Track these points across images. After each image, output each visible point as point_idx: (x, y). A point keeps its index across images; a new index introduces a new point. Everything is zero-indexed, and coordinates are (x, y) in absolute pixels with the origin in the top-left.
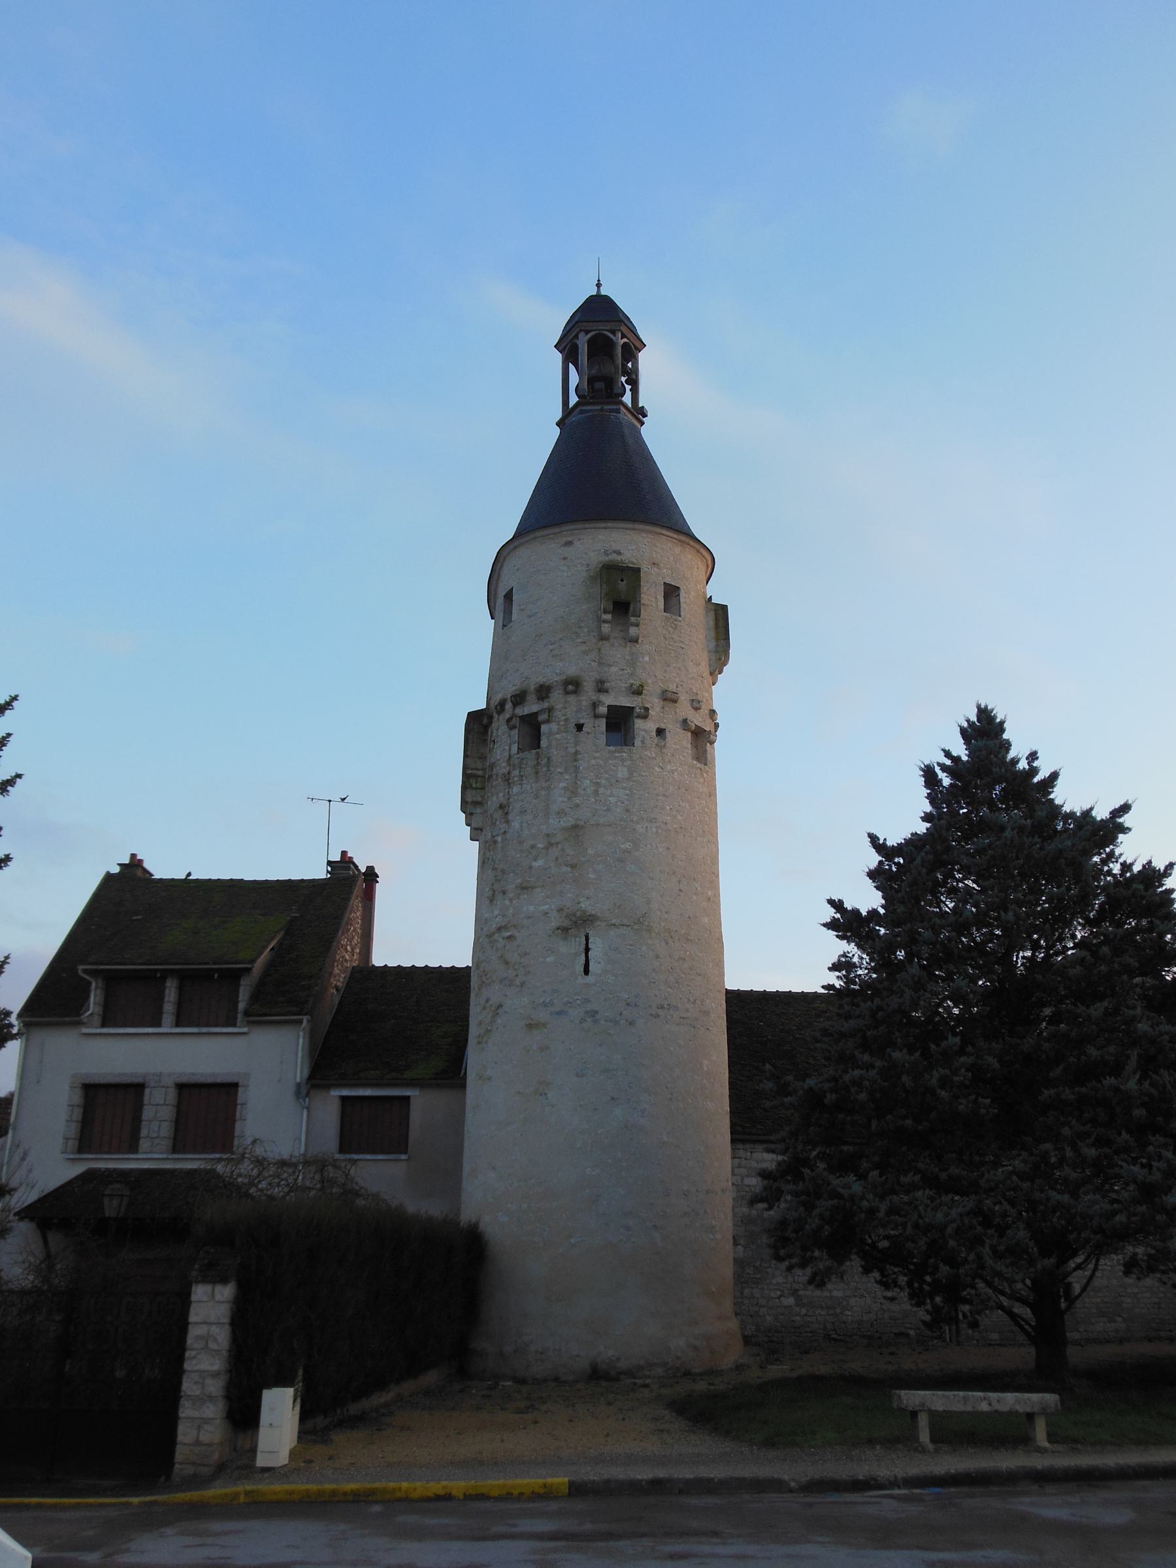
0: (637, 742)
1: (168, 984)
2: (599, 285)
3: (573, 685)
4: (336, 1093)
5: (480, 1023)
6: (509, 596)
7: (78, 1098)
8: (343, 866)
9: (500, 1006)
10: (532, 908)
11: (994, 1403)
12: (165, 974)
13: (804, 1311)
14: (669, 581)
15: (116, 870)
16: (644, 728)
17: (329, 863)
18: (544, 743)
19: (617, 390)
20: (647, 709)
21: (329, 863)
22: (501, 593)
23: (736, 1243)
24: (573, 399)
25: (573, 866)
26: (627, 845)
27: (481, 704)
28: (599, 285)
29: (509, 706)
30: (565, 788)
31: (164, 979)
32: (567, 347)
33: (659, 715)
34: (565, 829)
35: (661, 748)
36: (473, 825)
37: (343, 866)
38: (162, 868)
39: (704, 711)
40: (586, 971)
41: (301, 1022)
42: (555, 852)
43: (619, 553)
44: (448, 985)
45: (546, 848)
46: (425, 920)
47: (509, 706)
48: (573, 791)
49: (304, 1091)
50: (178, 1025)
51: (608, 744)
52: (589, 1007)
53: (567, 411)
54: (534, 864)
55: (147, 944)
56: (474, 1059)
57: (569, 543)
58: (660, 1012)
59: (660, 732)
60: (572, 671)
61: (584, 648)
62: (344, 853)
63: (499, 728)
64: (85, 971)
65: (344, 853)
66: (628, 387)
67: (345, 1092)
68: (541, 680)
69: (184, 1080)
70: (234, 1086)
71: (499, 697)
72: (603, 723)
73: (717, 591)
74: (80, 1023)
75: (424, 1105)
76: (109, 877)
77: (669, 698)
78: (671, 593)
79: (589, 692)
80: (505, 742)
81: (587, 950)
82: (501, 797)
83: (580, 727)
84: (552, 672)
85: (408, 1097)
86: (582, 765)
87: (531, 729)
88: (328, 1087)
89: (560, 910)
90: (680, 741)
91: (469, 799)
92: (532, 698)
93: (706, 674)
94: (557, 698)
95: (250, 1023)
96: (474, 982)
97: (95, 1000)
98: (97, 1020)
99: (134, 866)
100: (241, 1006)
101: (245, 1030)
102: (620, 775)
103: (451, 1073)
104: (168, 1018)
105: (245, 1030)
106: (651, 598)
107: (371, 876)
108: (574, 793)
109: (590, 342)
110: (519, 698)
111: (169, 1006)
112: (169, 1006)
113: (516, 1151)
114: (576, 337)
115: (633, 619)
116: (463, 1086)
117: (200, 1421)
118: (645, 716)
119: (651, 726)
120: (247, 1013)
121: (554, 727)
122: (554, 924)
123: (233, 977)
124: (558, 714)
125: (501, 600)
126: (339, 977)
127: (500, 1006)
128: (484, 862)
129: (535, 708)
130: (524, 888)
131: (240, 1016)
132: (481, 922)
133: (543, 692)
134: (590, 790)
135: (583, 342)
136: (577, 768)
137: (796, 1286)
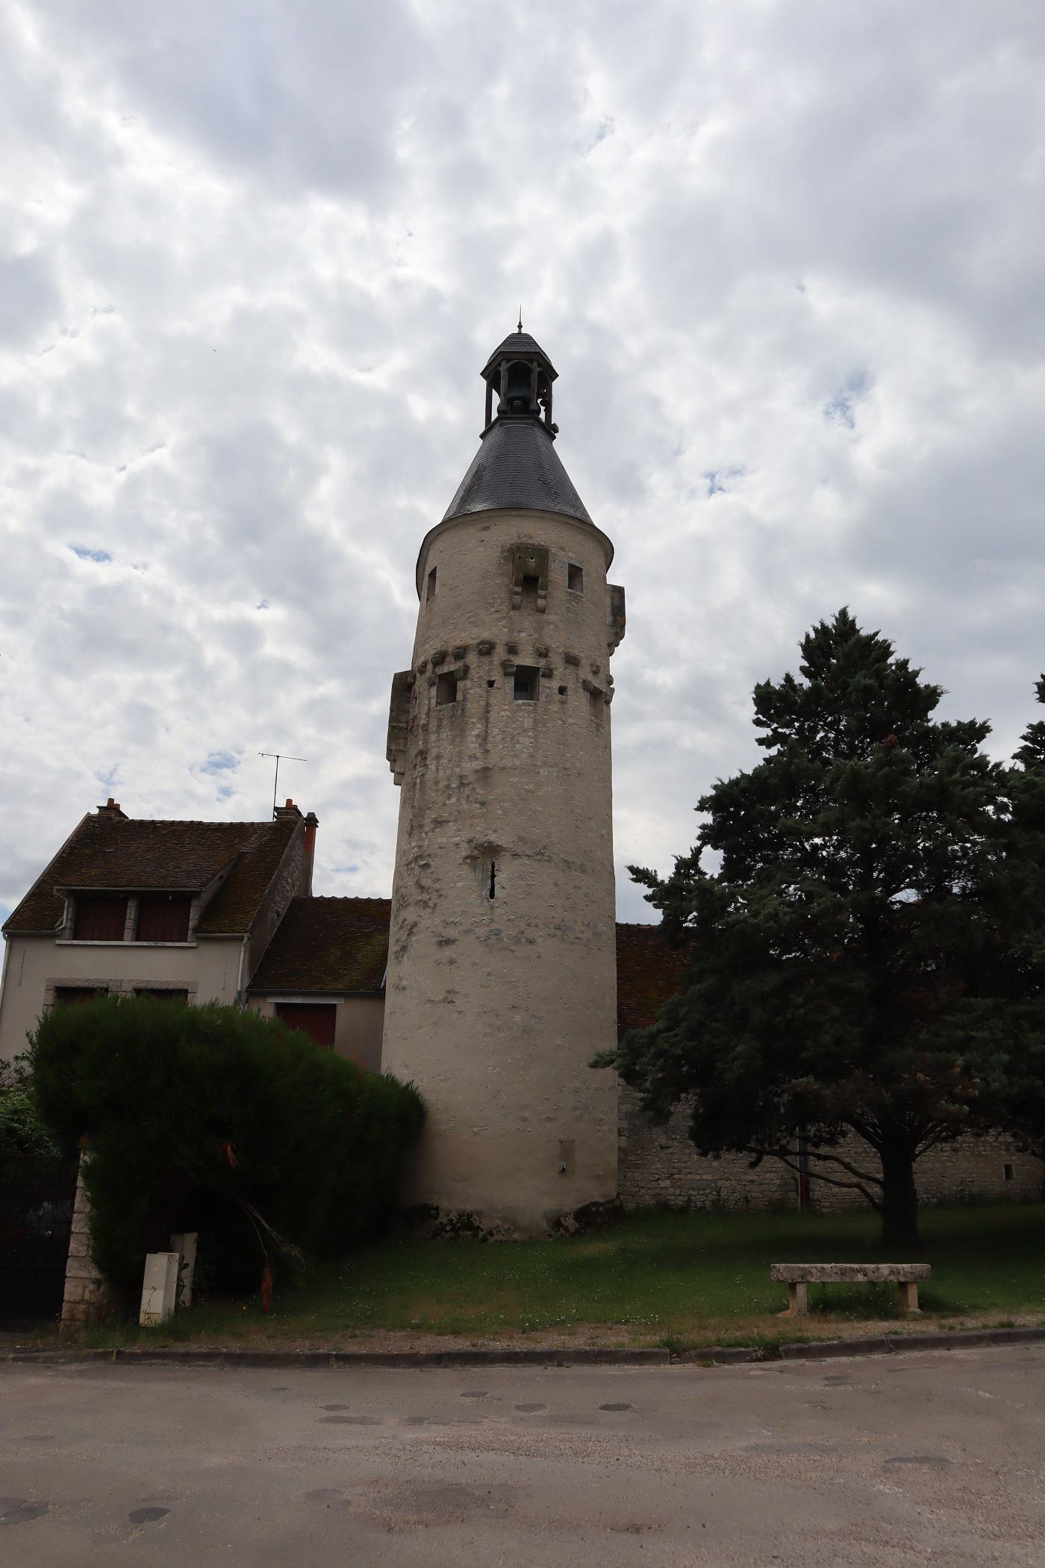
0: (542, 698)
1: (130, 904)
2: (520, 326)
3: (486, 649)
4: (272, 1000)
5: (398, 941)
6: (433, 575)
7: (50, 998)
8: (288, 814)
9: (415, 924)
10: (445, 840)
11: (870, 1274)
12: (129, 895)
13: (678, 1192)
14: (572, 562)
15: (95, 812)
16: (548, 687)
17: (276, 809)
18: (459, 696)
19: (533, 407)
20: (551, 670)
21: (276, 809)
22: (428, 571)
23: (620, 1134)
24: (495, 415)
25: (483, 804)
26: (531, 787)
27: (406, 666)
28: (520, 326)
29: (430, 666)
30: (478, 736)
31: (126, 900)
32: (492, 375)
33: (562, 674)
34: (477, 771)
35: (563, 703)
36: (397, 769)
37: (288, 814)
38: (134, 810)
39: (602, 675)
40: (492, 895)
41: (242, 939)
42: (467, 791)
43: (531, 537)
44: (369, 915)
45: (458, 787)
46: (356, 859)
47: (430, 666)
48: (484, 738)
49: (244, 997)
50: (137, 940)
51: (516, 698)
52: (494, 926)
53: (490, 425)
54: (535, 364)
55: (118, 873)
56: (392, 974)
57: (487, 528)
58: (558, 932)
59: (562, 690)
60: (486, 635)
61: (497, 616)
62: (289, 801)
63: (420, 683)
64: (59, 890)
65: (289, 801)
66: (543, 408)
67: (280, 1000)
68: (458, 643)
69: (142, 986)
70: (186, 992)
71: (422, 659)
72: (512, 681)
73: (615, 577)
74: (56, 936)
75: (348, 1014)
76: (89, 818)
77: (571, 661)
78: (575, 573)
79: (500, 653)
80: (427, 696)
81: (493, 876)
82: (421, 745)
83: (491, 684)
84: (469, 636)
85: (335, 1005)
86: (493, 716)
87: (448, 686)
88: (265, 995)
89: (470, 841)
90: (579, 701)
91: (393, 748)
92: (449, 658)
93: (604, 645)
94: (472, 658)
95: (198, 939)
96: (394, 907)
97: (66, 920)
98: (68, 932)
99: (111, 809)
100: (191, 924)
101: (194, 944)
102: (526, 725)
103: (371, 989)
104: (128, 933)
105: (194, 944)
106: (558, 575)
107: (312, 821)
108: (485, 740)
109: (510, 370)
110: (440, 659)
111: (129, 924)
112: (129, 924)
113: (426, 1037)
114: (499, 365)
115: (542, 593)
116: (379, 995)
117: (80, 1281)
118: (549, 674)
119: (555, 684)
120: (195, 930)
121: (468, 683)
122: (464, 854)
123: (184, 900)
124: (473, 672)
125: (427, 579)
126: (282, 906)
127: (415, 924)
128: (405, 802)
129: (452, 668)
130: (439, 823)
131: (190, 932)
132: (401, 853)
133: (460, 654)
134: (499, 738)
135: (504, 368)
136: (487, 719)
137: (672, 1171)
